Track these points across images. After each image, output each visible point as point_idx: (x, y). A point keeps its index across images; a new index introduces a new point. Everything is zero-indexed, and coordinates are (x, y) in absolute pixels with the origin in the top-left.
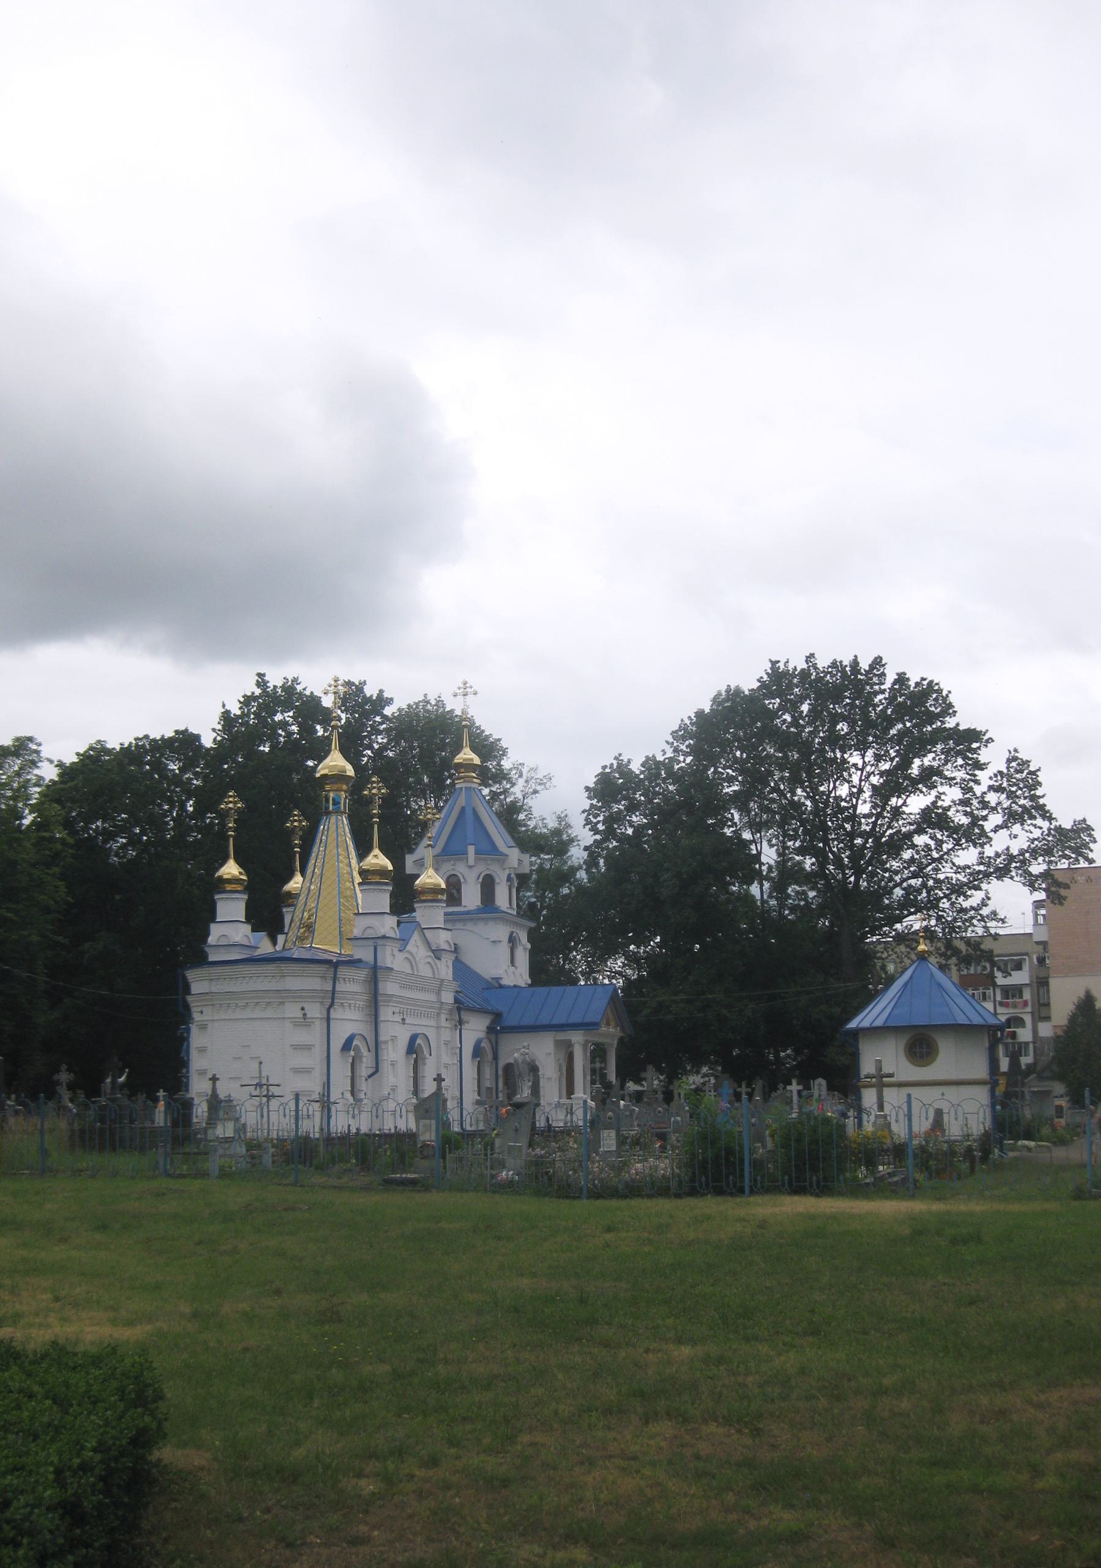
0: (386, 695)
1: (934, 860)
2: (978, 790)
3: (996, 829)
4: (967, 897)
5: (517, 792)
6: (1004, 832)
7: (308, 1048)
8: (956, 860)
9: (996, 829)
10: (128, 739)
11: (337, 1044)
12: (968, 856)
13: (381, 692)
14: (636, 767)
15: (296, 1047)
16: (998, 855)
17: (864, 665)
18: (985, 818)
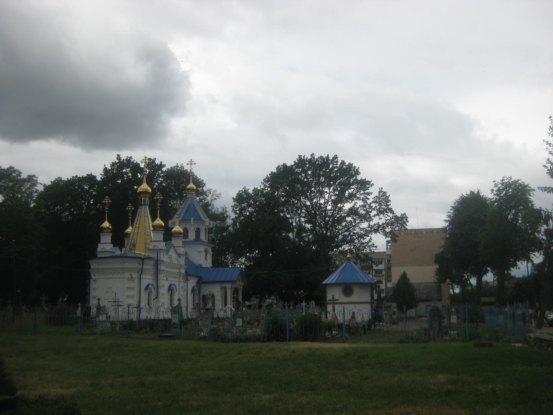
0: (163, 163)
1: (353, 226)
2: (369, 202)
3: (375, 216)
4: (364, 239)
5: (209, 199)
6: (377, 217)
7: (133, 288)
8: (361, 226)
9: (375, 216)
10: (70, 177)
11: (143, 288)
12: (365, 225)
13: (161, 162)
14: (250, 191)
15: (129, 288)
16: (375, 225)
17: (331, 158)
18: (371, 212)
